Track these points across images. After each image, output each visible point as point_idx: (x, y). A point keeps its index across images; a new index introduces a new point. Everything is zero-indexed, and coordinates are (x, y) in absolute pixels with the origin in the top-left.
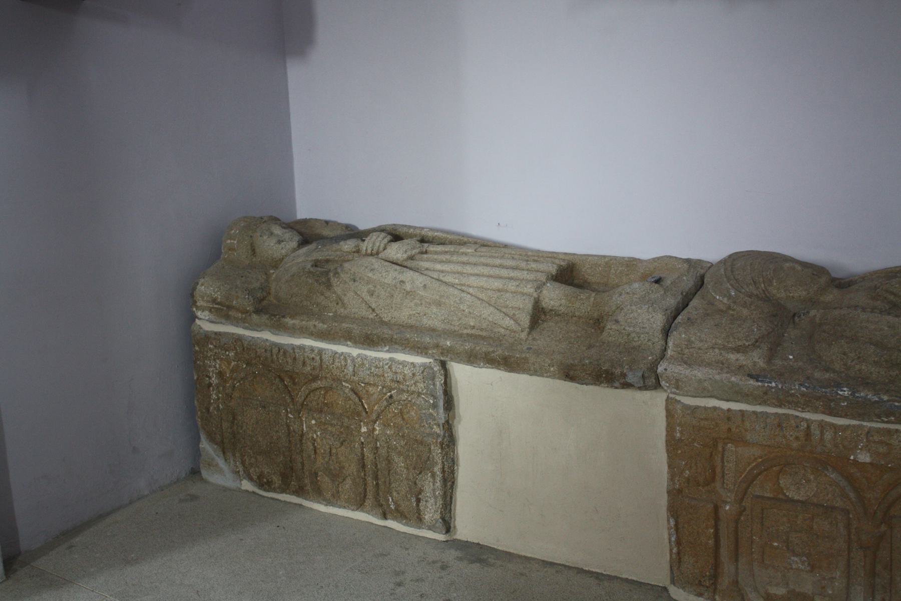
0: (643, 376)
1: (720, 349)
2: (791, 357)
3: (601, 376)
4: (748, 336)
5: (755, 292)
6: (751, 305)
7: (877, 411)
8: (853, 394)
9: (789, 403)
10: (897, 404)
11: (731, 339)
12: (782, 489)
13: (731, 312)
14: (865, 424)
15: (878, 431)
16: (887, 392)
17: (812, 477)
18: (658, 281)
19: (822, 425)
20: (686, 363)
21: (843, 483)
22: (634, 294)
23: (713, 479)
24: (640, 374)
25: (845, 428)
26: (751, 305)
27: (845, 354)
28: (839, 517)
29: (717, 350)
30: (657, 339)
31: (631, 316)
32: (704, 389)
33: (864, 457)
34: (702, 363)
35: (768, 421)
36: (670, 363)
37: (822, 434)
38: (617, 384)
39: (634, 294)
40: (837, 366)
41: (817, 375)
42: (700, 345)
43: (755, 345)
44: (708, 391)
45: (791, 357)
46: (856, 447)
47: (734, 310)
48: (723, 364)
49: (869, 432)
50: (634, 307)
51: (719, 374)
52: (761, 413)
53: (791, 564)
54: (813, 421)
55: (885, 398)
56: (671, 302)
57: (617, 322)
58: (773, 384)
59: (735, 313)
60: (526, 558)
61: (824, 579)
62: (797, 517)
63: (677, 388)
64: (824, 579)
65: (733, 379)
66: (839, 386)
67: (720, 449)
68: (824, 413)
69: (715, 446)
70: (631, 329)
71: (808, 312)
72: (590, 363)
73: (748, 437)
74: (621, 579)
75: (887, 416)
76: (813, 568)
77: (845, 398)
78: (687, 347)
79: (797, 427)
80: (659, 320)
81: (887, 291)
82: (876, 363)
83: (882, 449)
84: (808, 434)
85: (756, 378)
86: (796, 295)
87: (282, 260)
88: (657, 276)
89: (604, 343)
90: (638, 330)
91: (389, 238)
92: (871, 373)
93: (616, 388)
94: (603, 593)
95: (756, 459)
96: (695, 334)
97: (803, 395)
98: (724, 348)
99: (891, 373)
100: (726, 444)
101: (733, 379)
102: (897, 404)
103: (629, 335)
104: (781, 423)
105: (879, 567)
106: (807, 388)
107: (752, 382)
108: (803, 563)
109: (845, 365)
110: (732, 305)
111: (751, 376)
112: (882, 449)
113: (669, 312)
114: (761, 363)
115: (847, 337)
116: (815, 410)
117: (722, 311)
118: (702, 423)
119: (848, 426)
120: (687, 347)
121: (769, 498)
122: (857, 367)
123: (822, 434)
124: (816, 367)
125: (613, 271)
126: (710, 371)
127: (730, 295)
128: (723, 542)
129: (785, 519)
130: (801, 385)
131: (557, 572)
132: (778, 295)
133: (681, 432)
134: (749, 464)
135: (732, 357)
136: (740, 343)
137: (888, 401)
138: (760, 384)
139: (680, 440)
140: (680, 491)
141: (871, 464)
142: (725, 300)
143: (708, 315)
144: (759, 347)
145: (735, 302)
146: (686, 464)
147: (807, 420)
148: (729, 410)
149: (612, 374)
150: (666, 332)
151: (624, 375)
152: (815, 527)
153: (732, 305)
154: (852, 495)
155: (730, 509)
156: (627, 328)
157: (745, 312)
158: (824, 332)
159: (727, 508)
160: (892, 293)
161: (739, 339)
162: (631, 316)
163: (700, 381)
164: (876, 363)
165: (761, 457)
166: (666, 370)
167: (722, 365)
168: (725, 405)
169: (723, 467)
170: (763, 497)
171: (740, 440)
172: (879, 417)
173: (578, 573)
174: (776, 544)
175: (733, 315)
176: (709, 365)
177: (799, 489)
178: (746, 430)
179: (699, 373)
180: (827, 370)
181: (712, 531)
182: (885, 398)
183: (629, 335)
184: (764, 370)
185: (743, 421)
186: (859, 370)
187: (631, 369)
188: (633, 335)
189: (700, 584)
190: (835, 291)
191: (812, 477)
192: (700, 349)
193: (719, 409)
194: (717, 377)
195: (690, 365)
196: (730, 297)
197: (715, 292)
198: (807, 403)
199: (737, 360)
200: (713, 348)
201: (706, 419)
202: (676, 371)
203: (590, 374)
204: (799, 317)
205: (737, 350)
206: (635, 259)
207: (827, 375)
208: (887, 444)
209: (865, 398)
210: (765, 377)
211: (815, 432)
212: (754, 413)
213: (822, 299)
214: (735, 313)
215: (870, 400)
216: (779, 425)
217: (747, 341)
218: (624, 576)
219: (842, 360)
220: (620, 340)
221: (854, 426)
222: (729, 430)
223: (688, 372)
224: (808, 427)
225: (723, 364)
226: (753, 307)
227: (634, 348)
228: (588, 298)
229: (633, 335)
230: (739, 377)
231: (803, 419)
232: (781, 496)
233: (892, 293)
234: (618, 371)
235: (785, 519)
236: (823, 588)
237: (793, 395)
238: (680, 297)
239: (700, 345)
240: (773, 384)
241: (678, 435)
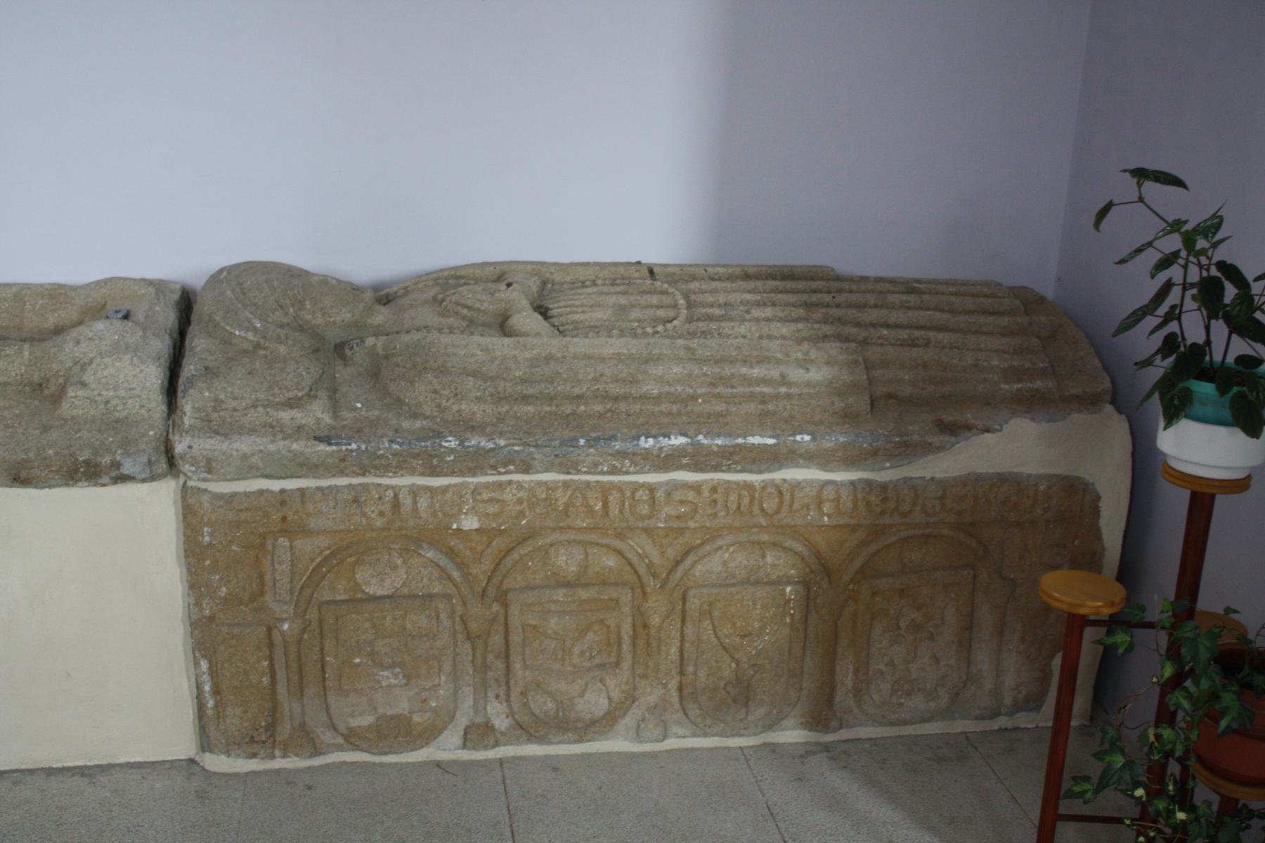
0: (149, 461)
1: (265, 407)
2: (359, 405)
3: (76, 471)
4: (298, 383)
5: (285, 320)
6: (287, 338)
7: (492, 461)
8: (461, 443)
9: (376, 467)
10: (516, 448)
11: (276, 390)
12: (360, 585)
13: (262, 352)
14: (470, 480)
15: (486, 486)
16: (501, 434)
17: (399, 562)
18: (126, 317)
19: (415, 492)
20: (217, 433)
21: (443, 561)
22: (100, 339)
23: (262, 592)
24: (145, 460)
25: (445, 489)
26: (287, 338)
27: (435, 392)
28: (441, 606)
29: (260, 409)
30: (154, 404)
31: (106, 373)
32: (251, 467)
33: (470, 523)
34: (242, 430)
35: (339, 497)
36: (193, 436)
37: (415, 502)
38: (105, 479)
39: (100, 339)
40: (427, 410)
41: (406, 424)
42: (234, 404)
44: (258, 469)
46: (460, 510)
47: (265, 349)
48: (272, 427)
49: (476, 491)
50: (107, 360)
51: (272, 442)
52: (330, 487)
53: (379, 682)
54: (400, 488)
55: (502, 442)
56: (162, 346)
57: (84, 385)
58: (354, 446)
59: (268, 352)
60: (153, 763)
61: (424, 689)
62: (385, 617)
63: (209, 471)
64: (424, 689)
65: (295, 446)
66: (440, 435)
67: (270, 548)
68: (423, 474)
69: (263, 545)
70: (111, 393)
71: (363, 342)
72: (57, 453)
73: (313, 523)
74: (119, 765)
75: (505, 465)
76: (408, 678)
77: (452, 451)
78: (215, 409)
79: (380, 498)
80: (154, 376)
81: (457, 304)
82: (478, 399)
83: (491, 509)
84: (396, 504)
85: (327, 440)
86: (338, 319)
88: (125, 306)
89: (66, 420)
90: (122, 393)
92: (474, 413)
93: (104, 485)
94: (108, 794)
95: (322, 551)
96: (224, 389)
97: (395, 454)
98: (269, 404)
100: (276, 539)
101: (295, 446)
102: (516, 448)
103: (107, 403)
104: (357, 498)
105: (490, 657)
106: (401, 444)
107: (323, 447)
108: (396, 676)
109: (439, 406)
110: (262, 341)
111: (319, 439)
112: (491, 509)
113: (162, 360)
114: (327, 419)
116: (413, 472)
117: (245, 351)
118: (243, 516)
119: (448, 487)
120: (215, 409)
121: (343, 601)
122: (455, 408)
123: (415, 502)
124: (399, 415)
125: (28, 306)
128: (281, 675)
129: (367, 625)
130: (392, 441)
131: (14, 783)
132: (314, 322)
133: (211, 534)
134: (312, 560)
135: (285, 415)
136: (291, 395)
137: (506, 446)
138: (334, 448)
139: (210, 545)
140: (212, 618)
141: (477, 530)
142: (250, 336)
143: (232, 359)
144: (316, 397)
145: (264, 337)
146: (222, 578)
147: (393, 487)
148: (282, 491)
149: (97, 465)
150: (171, 390)
151: (116, 465)
152: (409, 625)
153: (262, 341)
154: (456, 574)
155: (290, 627)
156: (104, 393)
157: (282, 349)
158: (398, 365)
159: (286, 626)
160: (465, 306)
161: (289, 390)
162: (106, 373)
163: (245, 457)
164: (478, 399)
165: (329, 548)
166: (190, 447)
167: (273, 429)
168: (275, 485)
169: (274, 571)
170: (334, 602)
171: (289, 529)
172: (494, 468)
173: (48, 776)
174: (357, 660)
175: (266, 356)
176: (253, 431)
177: (382, 580)
178: (308, 515)
179: (244, 445)
180: (415, 416)
181: (266, 663)
182: (502, 442)
183: (107, 403)
184: (333, 428)
185: (303, 502)
186: (459, 411)
187: (128, 454)
188: (114, 402)
189: (252, 740)
190: (383, 309)
191: (399, 562)
192: (235, 410)
193: (267, 491)
194: (272, 448)
195: (225, 436)
196: (255, 330)
198: (401, 464)
200: (255, 406)
201: (247, 509)
202: (207, 446)
203: (57, 472)
204: (352, 348)
205: (289, 404)
206: (61, 286)
207: (418, 424)
208: (498, 501)
209: (478, 446)
210: (340, 437)
211: (406, 500)
212: (318, 489)
213: (369, 321)
214: (268, 352)
215: (483, 448)
216: (355, 501)
217: (299, 390)
218: (122, 760)
220: (92, 412)
221: (456, 485)
222: (284, 518)
223: (225, 446)
224: (396, 496)
225: (272, 427)
227: (118, 421)
228: (20, 352)
229: (114, 402)
230: (303, 443)
231: (388, 487)
232: (359, 596)
233: (465, 306)
234: (106, 460)
235: (367, 625)
236: (424, 701)
237: (382, 456)
238: (167, 338)
239: (234, 404)
240: (354, 446)
241: (207, 539)
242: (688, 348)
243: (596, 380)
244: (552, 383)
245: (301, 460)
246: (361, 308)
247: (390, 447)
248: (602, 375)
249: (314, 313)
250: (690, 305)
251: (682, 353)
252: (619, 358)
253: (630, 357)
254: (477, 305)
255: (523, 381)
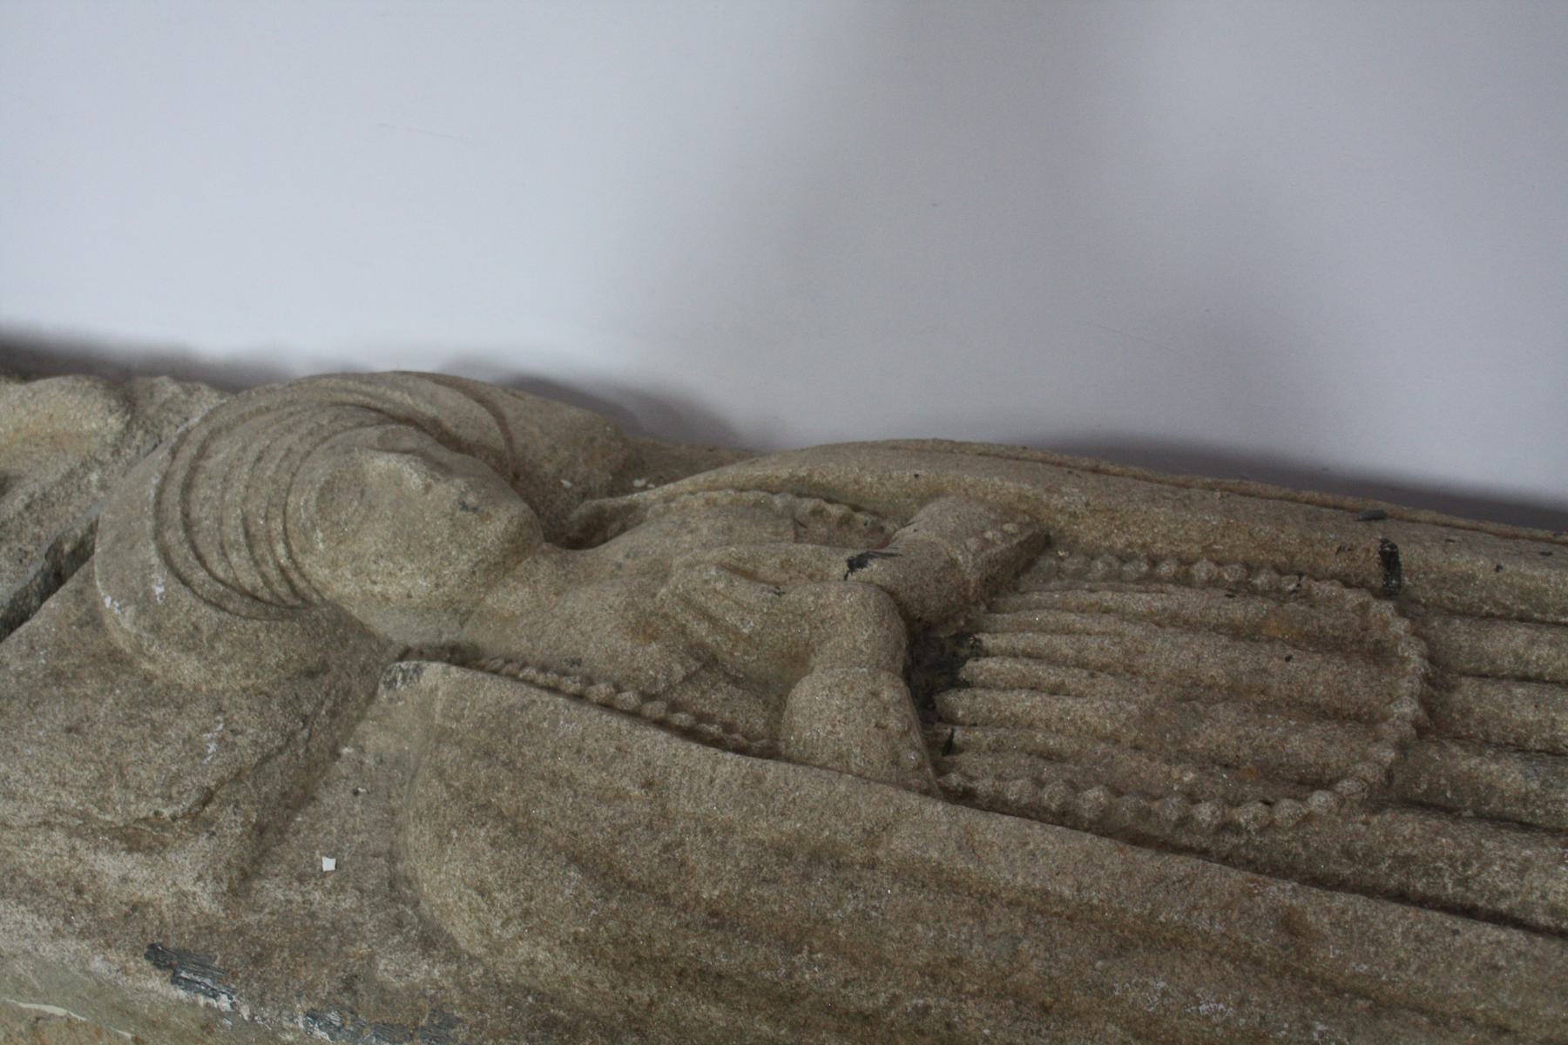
1: (72, 832)
4: (177, 777)
5: (249, 579)
6: (216, 636)
11: (115, 792)
26: (216, 636)
29: (58, 835)
43: (197, 820)
45: (328, 864)
47: (152, 659)
58: (224, 1003)
87: (882, 588)
91: (505, 517)
98: (85, 829)
99: (632, 991)
101: (97, 964)
107: (157, 983)
111: (159, 956)
114: (205, 901)
115: (501, 817)
122: (523, 949)
126: (30, 919)
127: (148, 594)
135: (111, 865)
136: (144, 809)
138: (182, 994)
145: (156, 628)
157: (189, 670)
161: (141, 795)
186: (531, 962)
194: (48, 950)
197: (107, 579)
199: (125, 880)
205: (132, 839)
210: (204, 967)
219: (473, 911)
225: (79, 891)
226: (221, 648)
240: (224, 1003)
242: (1290, 924)
243: (932, 973)
244: (792, 948)
245: (116, 999)
246: (464, 564)
247: (309, 1032)
248: (956, 962)
249: (334, 565)
250: (1436, 724)
251: (1264, 941)
252: (1038, 907)
253: (1077, 915)
254: (731, 619)
255: (717, 919)
